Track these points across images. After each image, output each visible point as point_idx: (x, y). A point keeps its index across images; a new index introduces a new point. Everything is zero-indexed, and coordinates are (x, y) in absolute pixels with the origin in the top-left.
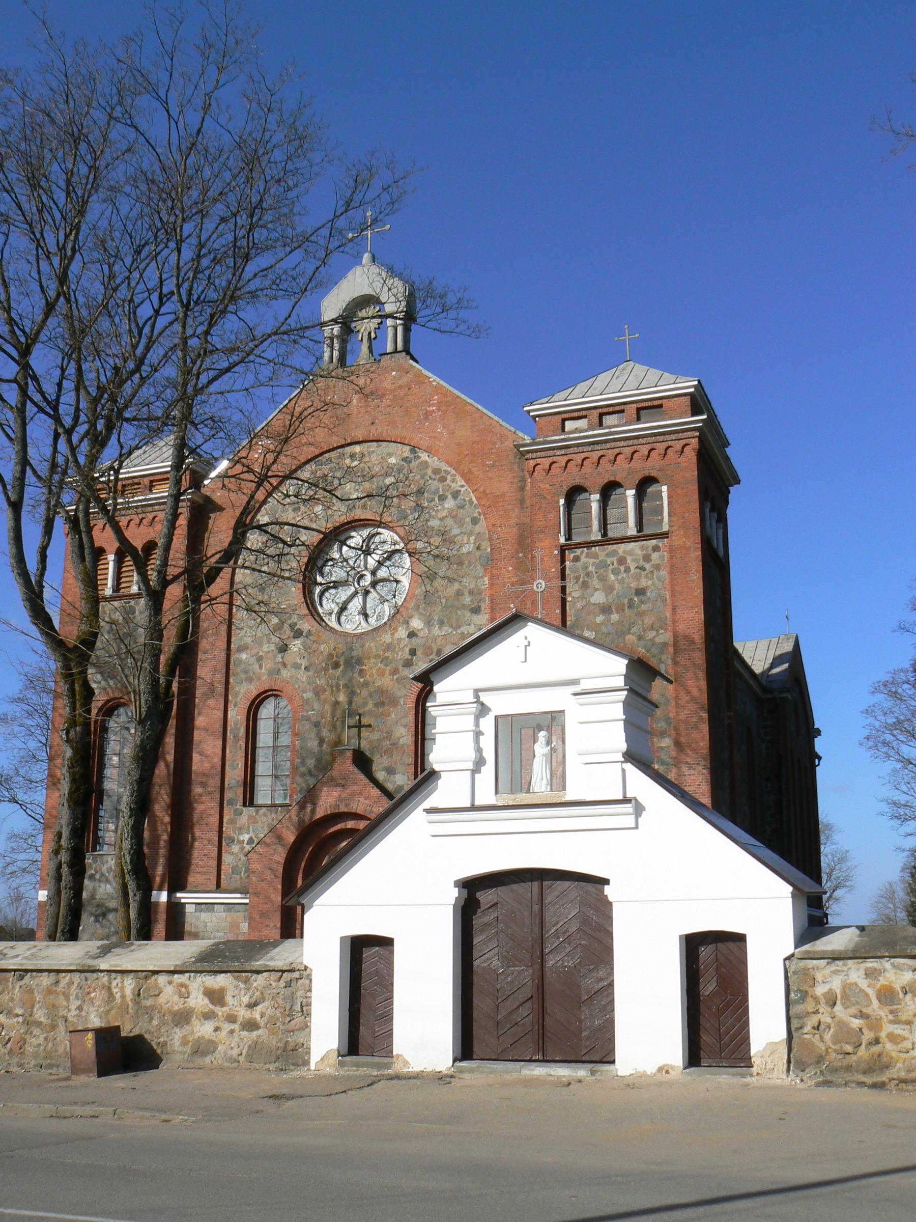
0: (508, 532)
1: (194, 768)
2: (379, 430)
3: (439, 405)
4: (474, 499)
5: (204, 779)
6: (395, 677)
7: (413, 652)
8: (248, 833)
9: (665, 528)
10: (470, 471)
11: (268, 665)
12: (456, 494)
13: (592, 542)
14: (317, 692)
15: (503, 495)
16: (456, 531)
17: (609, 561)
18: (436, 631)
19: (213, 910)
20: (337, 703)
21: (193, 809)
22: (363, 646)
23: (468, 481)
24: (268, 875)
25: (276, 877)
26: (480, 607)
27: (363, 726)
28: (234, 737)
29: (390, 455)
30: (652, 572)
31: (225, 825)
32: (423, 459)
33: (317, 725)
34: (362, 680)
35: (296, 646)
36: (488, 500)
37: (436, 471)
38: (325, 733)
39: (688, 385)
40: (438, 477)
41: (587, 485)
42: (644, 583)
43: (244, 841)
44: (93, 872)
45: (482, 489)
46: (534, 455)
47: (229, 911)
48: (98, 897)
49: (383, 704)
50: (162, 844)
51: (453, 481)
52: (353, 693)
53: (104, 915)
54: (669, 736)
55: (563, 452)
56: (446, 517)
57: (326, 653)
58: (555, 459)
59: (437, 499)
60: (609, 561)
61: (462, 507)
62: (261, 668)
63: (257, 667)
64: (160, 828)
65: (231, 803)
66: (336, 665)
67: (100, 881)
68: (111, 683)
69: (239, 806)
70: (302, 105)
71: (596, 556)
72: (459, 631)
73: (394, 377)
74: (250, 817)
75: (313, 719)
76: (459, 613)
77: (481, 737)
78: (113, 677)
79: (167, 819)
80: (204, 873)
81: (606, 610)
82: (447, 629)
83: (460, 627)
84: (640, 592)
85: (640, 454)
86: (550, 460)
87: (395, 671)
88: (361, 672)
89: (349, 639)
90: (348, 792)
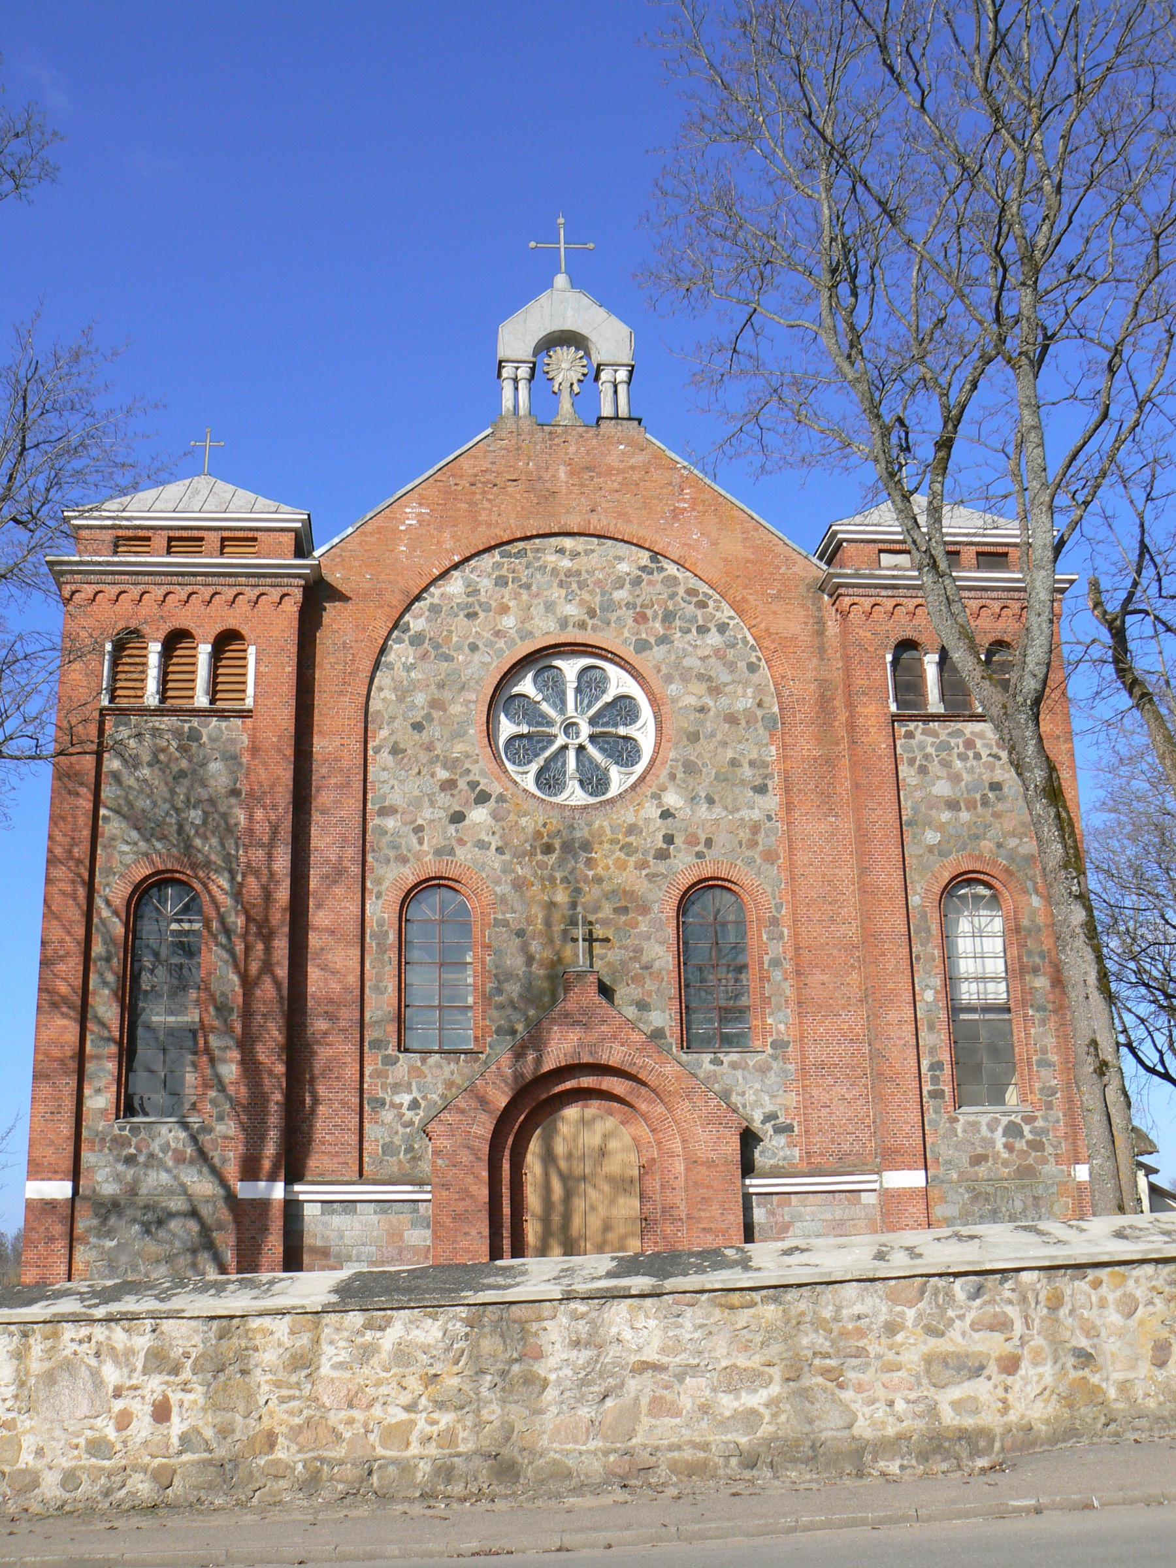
0: (804, 689)
1: (311, 989)
2: (604, 522)
3: (694, 502)
4: (750, 638)
5: (330, 1008)
6: (644, 873)
7: (669, 839)
8: (410, 1092)
9: (249, 703)
10: (744, 600)
12: (722, 628)
13: (932, 716)
14: (519, 885)
15: (794, 638)
17: (953, 742)
18: (703, 810)
19: (355, 1212)
20: (552, 905)
21: (313, 1053)
22: (590, 824)
23: (740, 613)
24: (465, 1157)
25: (478, 1159)
26: (766, 785)
27: (597, 940)
28: (378, 944)
29: (620, 559)
31: (367, 1079)
32: (668, 572)
33: (520, 933)
34: (591, 873)
35: (479, 815)
37: (692, 592)
38: (535, 946)
39: (292, 517)
40: (695, 600)
41: (922, 639)
43: (401, 1105)
44: (132, 1151)
45: (762, 626)
46: (851, 591)
47: (384, 1212)
48: (143, 1191)
49: (625, 910)
50: (273, 1107)
51: (718, 609)
52: (578, 891)
53: (160, 1223)
54: (1044, 974)
55: (890, 593)
56: (709, 656)
57: (530, 830)
58: (879, 600)
59: (694, 630)
60: (953, 742)
61: (733, 646)
62: (421, 842)
63: (415, 841)
64: (267, 1081)
65: (377, 1044)
66: (548, 849)
67: (146, 1166)
68: (159, 845)
69: (391, 1050)
70: (1157, 68)
71: (935, 734)
72: (737, 816)
73: (623, 453)
74: (412, 1069)
75: (514, 926)
76: (737, 790)
78: (163, 838)
79: (280, 1068)
80: (337, 1154)
81: (953, 805)
82: (718, 811)
83: (738, 810)
85: (83, 595)
86: (189, 589)
87: (642, 865)
88: (589, 862)
89: (567, 813)
90: (594, 1035)
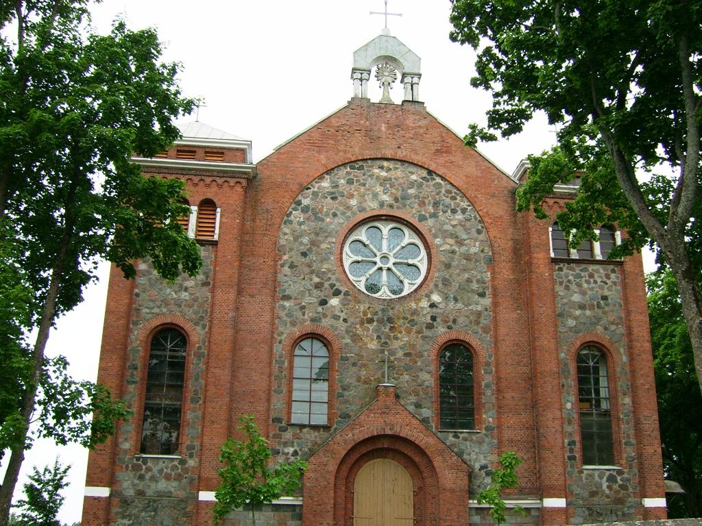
2: (404, 153)
7: (434, 318)
8: (293, 446)
9: (216, 238)
11: (309, 314)
12: (464, 211)
16: (465, 237)
17: (583, 274)
18: (452, 304)
30: (612, 286)
36: (490, 219)
40: (450, 195)
42: (606, 293)
45: (485, 210)
59: (449, 212)
60: (583, 274)
61: (469, 220)
72: (470, 308)
77: (67, 366)
83: (470, 305)
84: (605, 298)
